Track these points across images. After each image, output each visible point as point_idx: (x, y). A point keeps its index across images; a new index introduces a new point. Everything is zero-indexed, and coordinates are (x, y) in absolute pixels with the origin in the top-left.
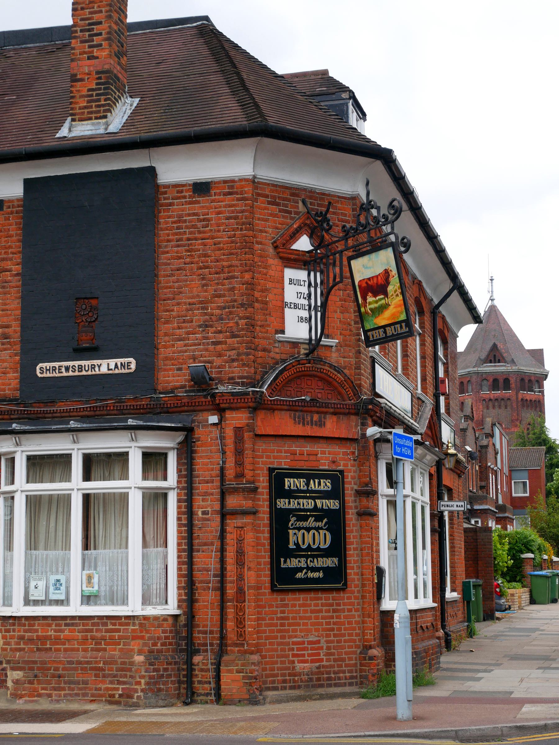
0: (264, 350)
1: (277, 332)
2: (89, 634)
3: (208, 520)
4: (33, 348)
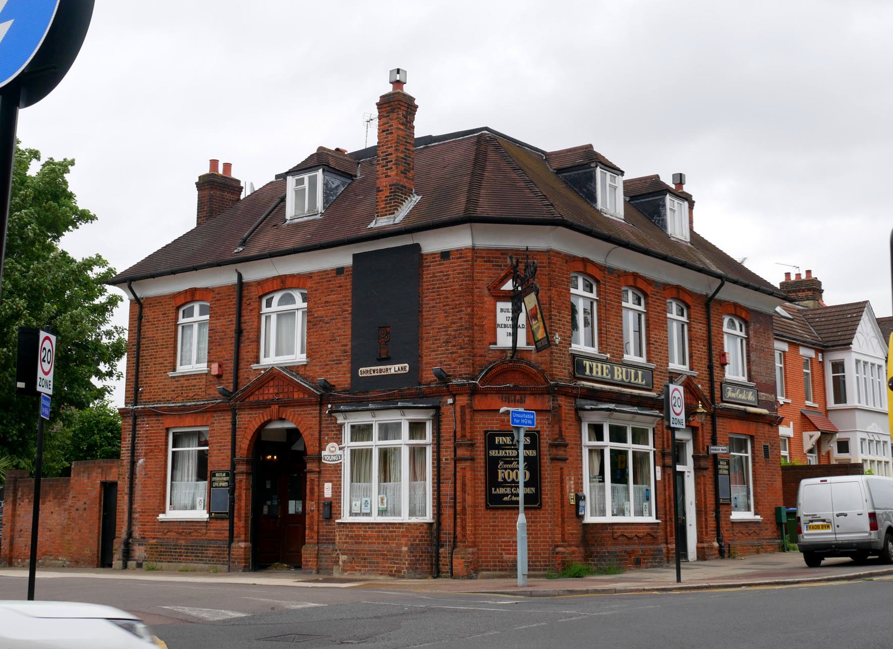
0: (481, 356)
1: (490, 344)
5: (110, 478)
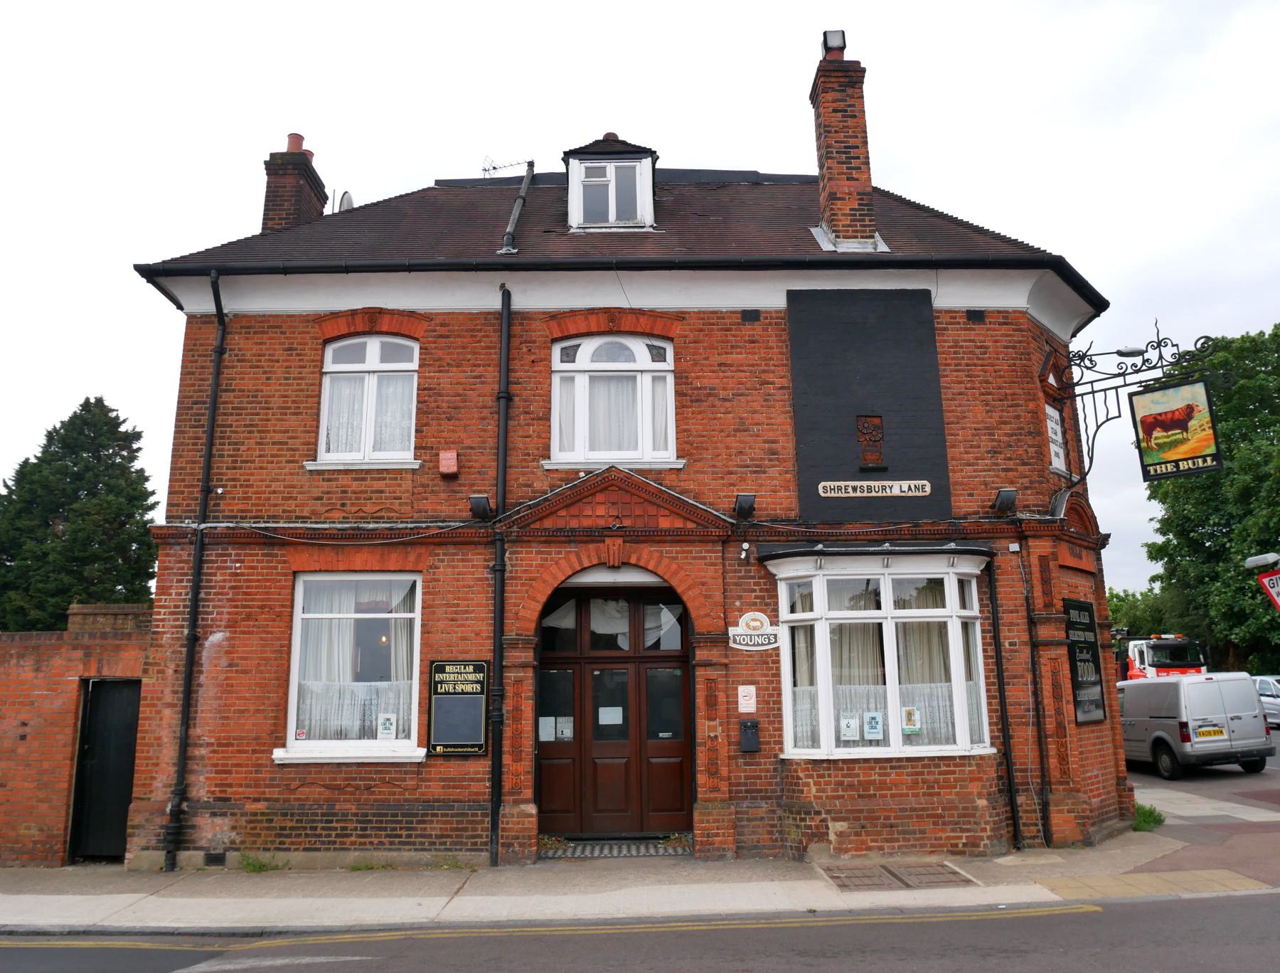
2: (920, 778)
3: (1016, 651)
4: (809, 470)
5: (117, 669)
